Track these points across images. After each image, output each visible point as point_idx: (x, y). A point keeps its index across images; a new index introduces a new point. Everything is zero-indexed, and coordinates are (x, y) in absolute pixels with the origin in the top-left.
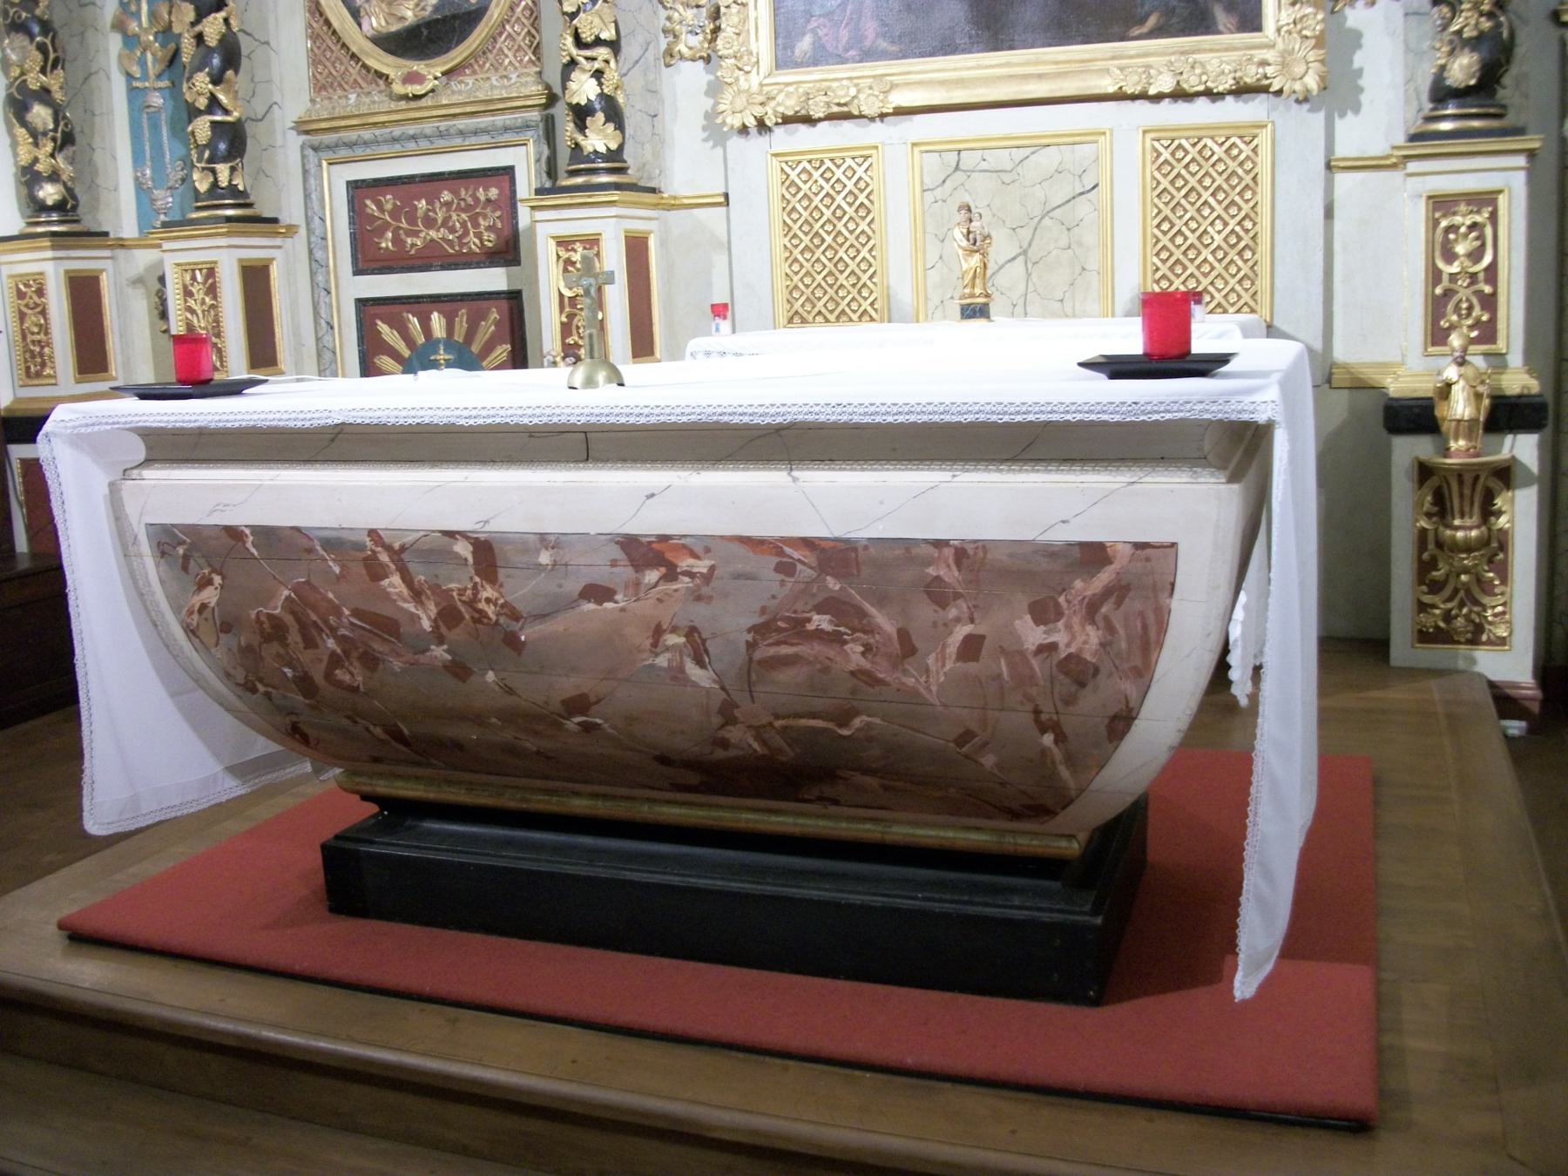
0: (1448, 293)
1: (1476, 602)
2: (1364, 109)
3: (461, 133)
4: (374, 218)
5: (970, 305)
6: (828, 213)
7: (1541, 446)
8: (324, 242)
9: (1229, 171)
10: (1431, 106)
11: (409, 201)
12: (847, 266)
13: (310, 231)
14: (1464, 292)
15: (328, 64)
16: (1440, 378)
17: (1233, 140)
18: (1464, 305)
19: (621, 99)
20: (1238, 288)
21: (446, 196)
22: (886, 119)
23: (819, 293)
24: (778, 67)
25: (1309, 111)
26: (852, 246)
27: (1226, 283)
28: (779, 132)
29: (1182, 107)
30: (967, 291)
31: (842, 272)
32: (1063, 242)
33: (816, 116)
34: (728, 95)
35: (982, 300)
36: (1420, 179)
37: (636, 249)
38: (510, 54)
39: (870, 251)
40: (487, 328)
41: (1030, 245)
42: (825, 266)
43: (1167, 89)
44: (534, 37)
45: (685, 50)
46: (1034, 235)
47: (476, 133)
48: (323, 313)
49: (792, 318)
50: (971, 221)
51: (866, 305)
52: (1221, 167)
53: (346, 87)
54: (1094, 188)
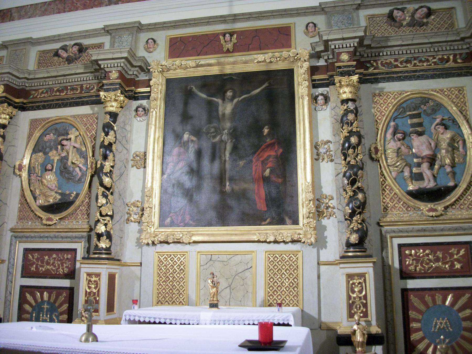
0: (353, 303)
2: (328, 248)
3: (62, 237)
4: (30, 260)
5: (212, 303)
6: (171, 271)
7: (383, 349)
8: (13, 266)
9: (290, 264)
10: (346, 248)
11: (42, 256)
12: (176, 287)
13: (9, 262)
14: (358, 302)
15: (24, 212)
17: (291, 255)
18: (358, 306)
19: (112, 232)
20: (293, 299)
21: (54, 256)
22: (191, 244)
23: (167, 295)
24: (160, 226)
25: (312, 248)
26: (178, 281)
27: (289, 297)
28: (159, 246)
29: (276, 245)
30: (212, 299)
31: (174, 289)
32: (242, 283)
33: (170, 242)
34: (144, 234)
35: (216, 302)
36: (344, 269)
37: (112, 278)
38: (80, 215)
39: (183, 283)
40: (62, 298)
41: (231, 284)
42: (169, 287)
43: (272, 240)
44: (88, 211)
45: (133, 219)
46: (233, 281)
47: (66, 238)
48: (9, 289)
49: (158, 302)
50: (214, 278)
51: (181, 300)
52: (288, 263)
53: (28, 219)
54: (251, 268)
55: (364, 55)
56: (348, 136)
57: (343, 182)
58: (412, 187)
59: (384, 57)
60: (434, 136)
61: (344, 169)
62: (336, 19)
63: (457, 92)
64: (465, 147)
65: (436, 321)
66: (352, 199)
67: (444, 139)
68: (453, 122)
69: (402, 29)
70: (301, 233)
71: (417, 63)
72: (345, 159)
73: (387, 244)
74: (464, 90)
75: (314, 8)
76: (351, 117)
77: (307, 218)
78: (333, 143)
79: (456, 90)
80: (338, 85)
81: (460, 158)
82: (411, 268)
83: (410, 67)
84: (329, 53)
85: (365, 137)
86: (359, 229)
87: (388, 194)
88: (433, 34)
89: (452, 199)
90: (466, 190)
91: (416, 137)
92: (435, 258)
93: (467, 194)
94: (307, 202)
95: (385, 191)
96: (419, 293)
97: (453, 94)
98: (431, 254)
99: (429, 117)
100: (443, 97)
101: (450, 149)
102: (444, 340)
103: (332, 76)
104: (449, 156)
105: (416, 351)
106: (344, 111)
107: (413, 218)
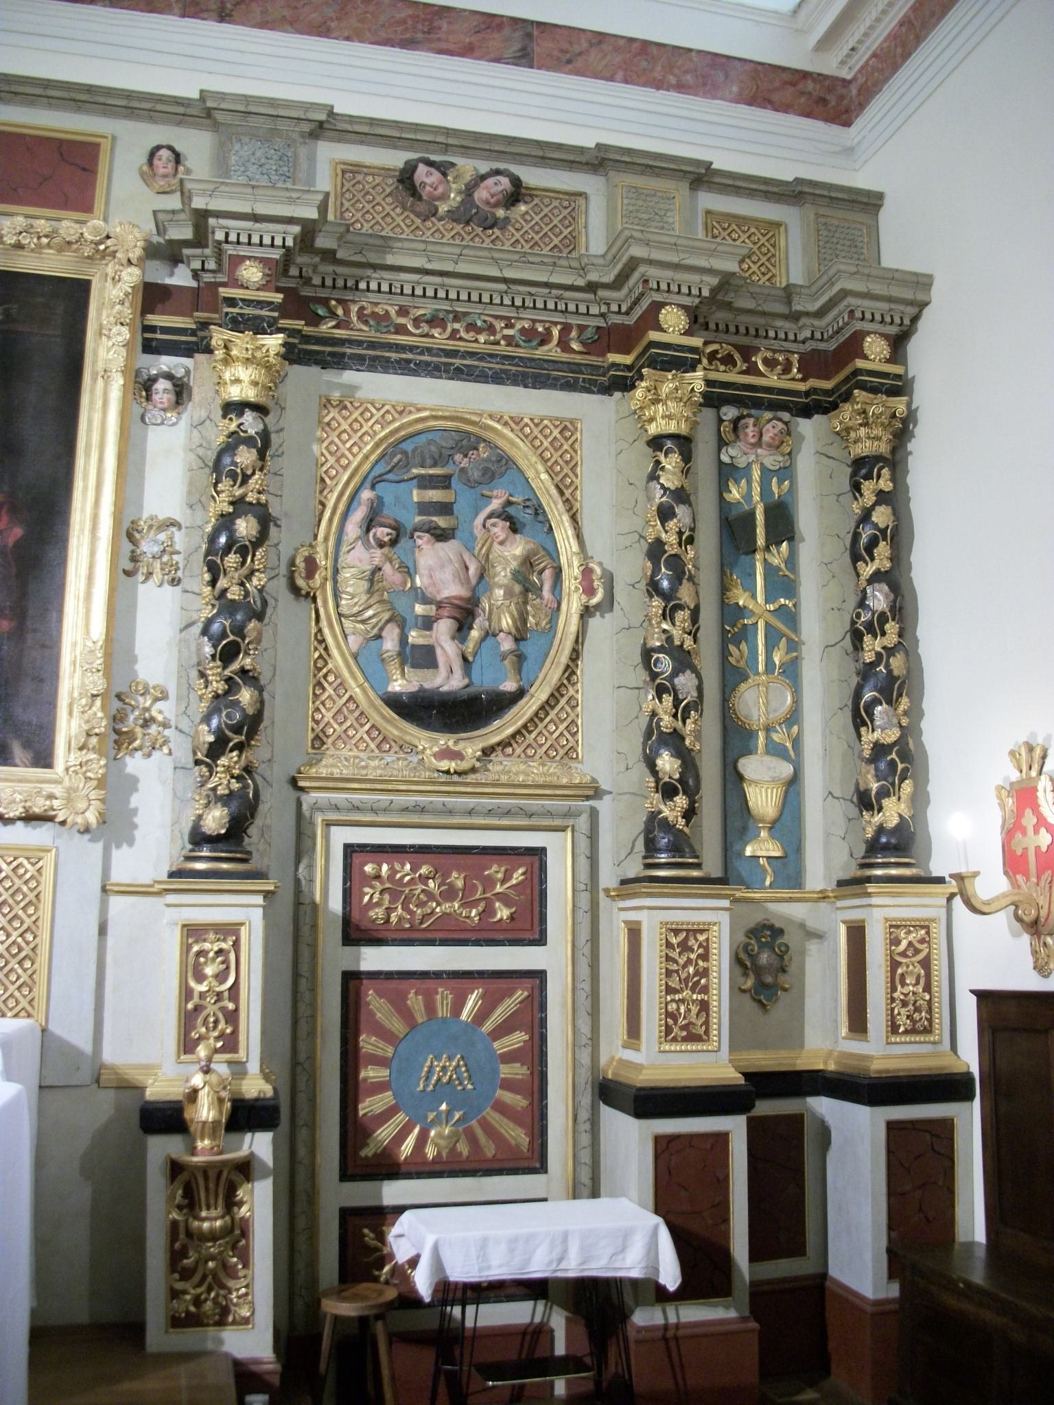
0: (197, 1009)
1: (223, 1286)
7: (275, 1143)
9: (15, 888)
10: (190, 847)
14: (211, 1008)
16: (188, 1085)
17: (21, 860)
18: (212, 1019)
20: (17, 994)
25: (90, 840)
36: (177, 909)
55: (311, 279)
56: (230, 513)
57: (199, 648)
58: (400, 686)
59: (369, 294)
60: (480, 546)
61: (208, 612)
62: (245, 152)
63: (556, 433)
64: (558, 587)
65: (432, 1062)
66: (221, 701)
67: (505, 558)
68: (537, 514)
69: (434, 224)
70: (58, 795)
71: (462, 330)
72: (213, 583)
73: (314, 844)
74: (576, 429)
75: (183, 105)
76: (246, 457)
77: (81, 749)
78: (183, 529)
79: (556, 427)
80: (219, 354)
81: (543, 616)
82: (377, 914)
83: (439, 338)
84: (208, 251)
85: (283, 523)
86: (231, 793)
87: (330, 697)
88: (516, 257)
89: (506, 729)
90: (547, 708)
91: (429, 542)
92: (443, 888)
93: (548, 719)
94: (84, 701)
95: (324, 689)
96: (393, 984)
97: (546, 437)
98: (433, 878)
99: (472, 491)
100: (518, 440)
101: (517, 588)
102: (449, 1113)
103: (204, 325)
104: (513, 607)
105: (372, 1145)
106: (229, 437)
107: (395, 773)
